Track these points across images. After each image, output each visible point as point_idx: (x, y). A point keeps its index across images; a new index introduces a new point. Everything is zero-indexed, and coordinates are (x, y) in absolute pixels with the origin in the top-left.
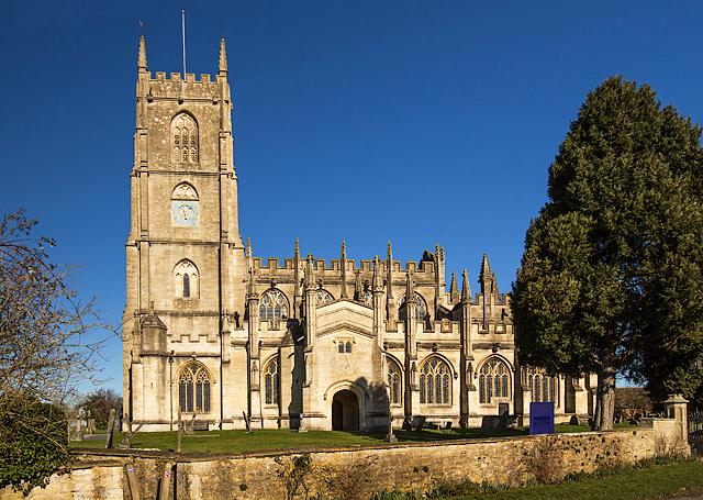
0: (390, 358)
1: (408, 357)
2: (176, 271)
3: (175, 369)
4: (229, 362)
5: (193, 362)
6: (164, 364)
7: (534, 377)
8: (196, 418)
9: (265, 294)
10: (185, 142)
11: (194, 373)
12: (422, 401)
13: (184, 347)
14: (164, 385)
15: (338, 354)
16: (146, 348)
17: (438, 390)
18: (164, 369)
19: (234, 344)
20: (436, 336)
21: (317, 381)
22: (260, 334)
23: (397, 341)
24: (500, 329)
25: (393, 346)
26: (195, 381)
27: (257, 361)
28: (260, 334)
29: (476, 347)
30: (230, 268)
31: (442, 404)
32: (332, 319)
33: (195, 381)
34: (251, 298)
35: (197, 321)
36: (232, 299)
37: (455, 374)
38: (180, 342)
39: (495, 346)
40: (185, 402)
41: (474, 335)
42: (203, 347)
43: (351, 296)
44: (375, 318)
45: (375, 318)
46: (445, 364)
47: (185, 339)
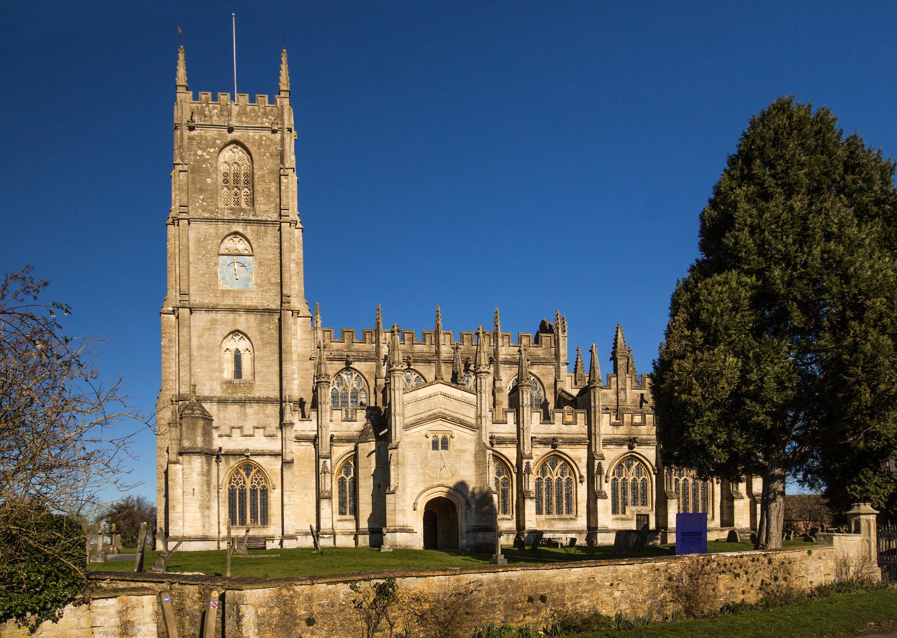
1: (520, 456)
2: (224, 347)
5: (246, 462)
7: (681, 482)
10: (237, 182)
11: (248, 475)
12: (539, 511)
14: (209, 491)
15: (431, 452)
16: (186, 444)
17: (559, 498)
19: (299, 439)
20: (556, 428)
22: (332, 427)
25: (502, 441)
26: (248, 486)
27: (328, 461)
29: (608, 442)
33: (248, 486)
34: (319, 382)
38: (229, 436)
39: (632, 442)
41: (605, 427)
42: (259, 442)
43: (448, 377)
44: (478, 406)
46: (568, 464)
47: (236, 433)
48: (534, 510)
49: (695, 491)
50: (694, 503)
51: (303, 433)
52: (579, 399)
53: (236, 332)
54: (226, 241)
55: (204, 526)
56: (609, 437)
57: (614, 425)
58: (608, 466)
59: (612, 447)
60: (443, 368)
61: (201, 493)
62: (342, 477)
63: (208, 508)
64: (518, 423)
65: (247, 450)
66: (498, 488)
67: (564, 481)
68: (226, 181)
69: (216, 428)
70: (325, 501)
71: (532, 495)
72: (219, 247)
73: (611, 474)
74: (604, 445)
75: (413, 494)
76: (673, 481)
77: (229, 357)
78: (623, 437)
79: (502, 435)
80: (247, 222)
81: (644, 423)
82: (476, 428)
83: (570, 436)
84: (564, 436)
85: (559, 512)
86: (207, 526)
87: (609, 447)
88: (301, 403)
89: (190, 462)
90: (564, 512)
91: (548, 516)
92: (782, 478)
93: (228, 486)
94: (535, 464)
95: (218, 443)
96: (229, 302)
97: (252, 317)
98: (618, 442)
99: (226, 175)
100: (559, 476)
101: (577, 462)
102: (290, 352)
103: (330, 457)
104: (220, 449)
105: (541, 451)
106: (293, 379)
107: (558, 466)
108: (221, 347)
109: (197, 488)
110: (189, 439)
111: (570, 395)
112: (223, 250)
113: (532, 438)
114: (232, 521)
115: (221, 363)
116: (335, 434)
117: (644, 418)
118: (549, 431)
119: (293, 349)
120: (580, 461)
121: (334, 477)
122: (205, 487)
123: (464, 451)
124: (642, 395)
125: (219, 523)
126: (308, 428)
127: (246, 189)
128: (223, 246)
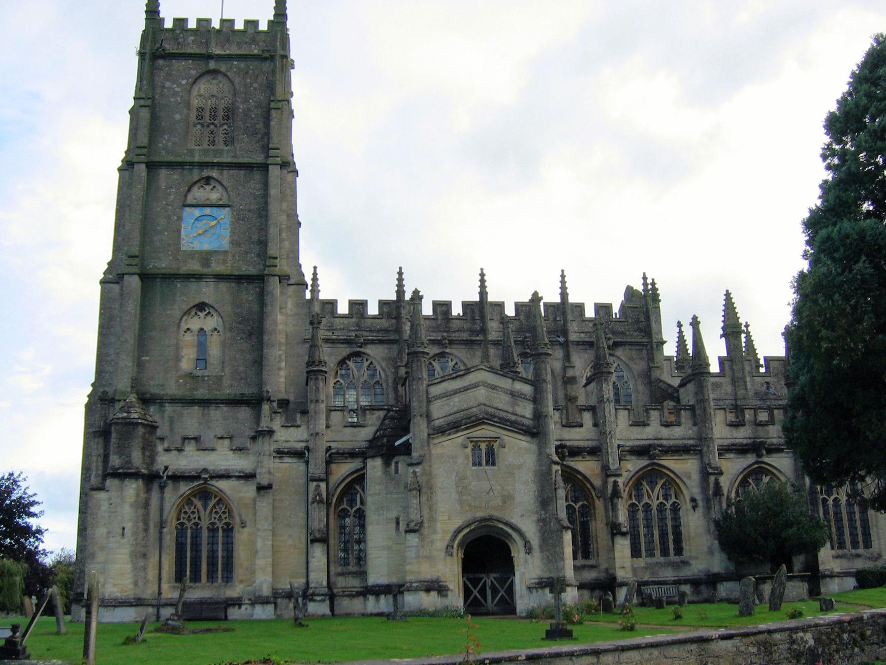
0: (570, 476)
1: (607, 472)
2: (184, 326)
3: (172, 496)
4: (269, 487)
5: (202, 486)
6: (148, 490)
7: (830, 502)
8: (566, 523)
9: (342, 363)
10: (214, 117)
11: (205, 506)
12: (636, 552)
13: (190, 460)
14: (146, 530)
15: (472, 470)
16: (115, 461)
17: (663, 535)
18: (146, 505)
19: (281, 453)
20: (653, 431)
21: (433, 520)
22: (329, 435)
23: (581, 444)
24: (763, 416)
25: (575, 452)
26: (205, 524)
27: (323, 485)
28: (329, 435)
29: (725, 450)
30: (280, 318)
31: (861, 551)
32: (457, 402)
33: (205, 524)
34: (313, 371)
35: (217, 414)
36: (282, 373)
37: (693, 500)
38: (180, 450)
39: (755, 448)
40: (186, 569)
41: (720, 430)
42: (222, 458)
43: (496, 363)
44: (537, 400)
45: (537, 400)
46: (672, 484)
47: (190, 448)
48: (628, 552)
49: (851, 520)
50: (851, 534)
51: (287, 445)
53: (201, 306)
54: (195, 189)
55: (136, 584)
56: (726, 442)
57: (732, 425)
58: (728, 483)
59: (732, 456)
60: (492, 351)
61: (135, 533)
62: (344, 509)
63: (144, 556)
64: (596, 425)
65: (205, 470)
66: (571, 520)
67: (668, 506)
68: (200, 117)
69: (162, 439)
71: (624, 530)
72: (186, 196)
73: (733, 495)
74: (720, 455)
75: (445, 532)
76: (820, 502)
77: (189, 339)
78: (745, 441)
79: (576, 443)
80: (221, 166)
81: (771, 421)
82: (535, 431)
83: (672, 443)
84: (665, 442)
85: (665, 552)
86: (140, 583)
87: (728, 456)
88: (284, 403)
89: (121, 489)
90: (484, 462)
91: (649, 560)
92: (862, 479)
93: (175, 523)
94: (626, 485)
95: (169, 461)
96: (195, 266)
97: (223, 286)
98: (741, 450)
99: (200, 110)
100: (661, 500)
101: (685, 479)
103: (326, 480)
104: (166, 468)
105: (633, 465)
106: (280, 369)
107: (659, 486)
108: (179, 326)
109: (129, 526)
110: (120, 454)
111: (670, 386)
112: (190, 199)
113: (619, 446)
114: (179, 577)
115: (178, 348)
116: (333, 445)
117: (771, 415)
118: (644, 436)
119: (280, 327)
120: (689, 478)
121: (332, 509)
123: (520, 467)
125: (160, 579)
126: (291, 436)
128: (190, 197)
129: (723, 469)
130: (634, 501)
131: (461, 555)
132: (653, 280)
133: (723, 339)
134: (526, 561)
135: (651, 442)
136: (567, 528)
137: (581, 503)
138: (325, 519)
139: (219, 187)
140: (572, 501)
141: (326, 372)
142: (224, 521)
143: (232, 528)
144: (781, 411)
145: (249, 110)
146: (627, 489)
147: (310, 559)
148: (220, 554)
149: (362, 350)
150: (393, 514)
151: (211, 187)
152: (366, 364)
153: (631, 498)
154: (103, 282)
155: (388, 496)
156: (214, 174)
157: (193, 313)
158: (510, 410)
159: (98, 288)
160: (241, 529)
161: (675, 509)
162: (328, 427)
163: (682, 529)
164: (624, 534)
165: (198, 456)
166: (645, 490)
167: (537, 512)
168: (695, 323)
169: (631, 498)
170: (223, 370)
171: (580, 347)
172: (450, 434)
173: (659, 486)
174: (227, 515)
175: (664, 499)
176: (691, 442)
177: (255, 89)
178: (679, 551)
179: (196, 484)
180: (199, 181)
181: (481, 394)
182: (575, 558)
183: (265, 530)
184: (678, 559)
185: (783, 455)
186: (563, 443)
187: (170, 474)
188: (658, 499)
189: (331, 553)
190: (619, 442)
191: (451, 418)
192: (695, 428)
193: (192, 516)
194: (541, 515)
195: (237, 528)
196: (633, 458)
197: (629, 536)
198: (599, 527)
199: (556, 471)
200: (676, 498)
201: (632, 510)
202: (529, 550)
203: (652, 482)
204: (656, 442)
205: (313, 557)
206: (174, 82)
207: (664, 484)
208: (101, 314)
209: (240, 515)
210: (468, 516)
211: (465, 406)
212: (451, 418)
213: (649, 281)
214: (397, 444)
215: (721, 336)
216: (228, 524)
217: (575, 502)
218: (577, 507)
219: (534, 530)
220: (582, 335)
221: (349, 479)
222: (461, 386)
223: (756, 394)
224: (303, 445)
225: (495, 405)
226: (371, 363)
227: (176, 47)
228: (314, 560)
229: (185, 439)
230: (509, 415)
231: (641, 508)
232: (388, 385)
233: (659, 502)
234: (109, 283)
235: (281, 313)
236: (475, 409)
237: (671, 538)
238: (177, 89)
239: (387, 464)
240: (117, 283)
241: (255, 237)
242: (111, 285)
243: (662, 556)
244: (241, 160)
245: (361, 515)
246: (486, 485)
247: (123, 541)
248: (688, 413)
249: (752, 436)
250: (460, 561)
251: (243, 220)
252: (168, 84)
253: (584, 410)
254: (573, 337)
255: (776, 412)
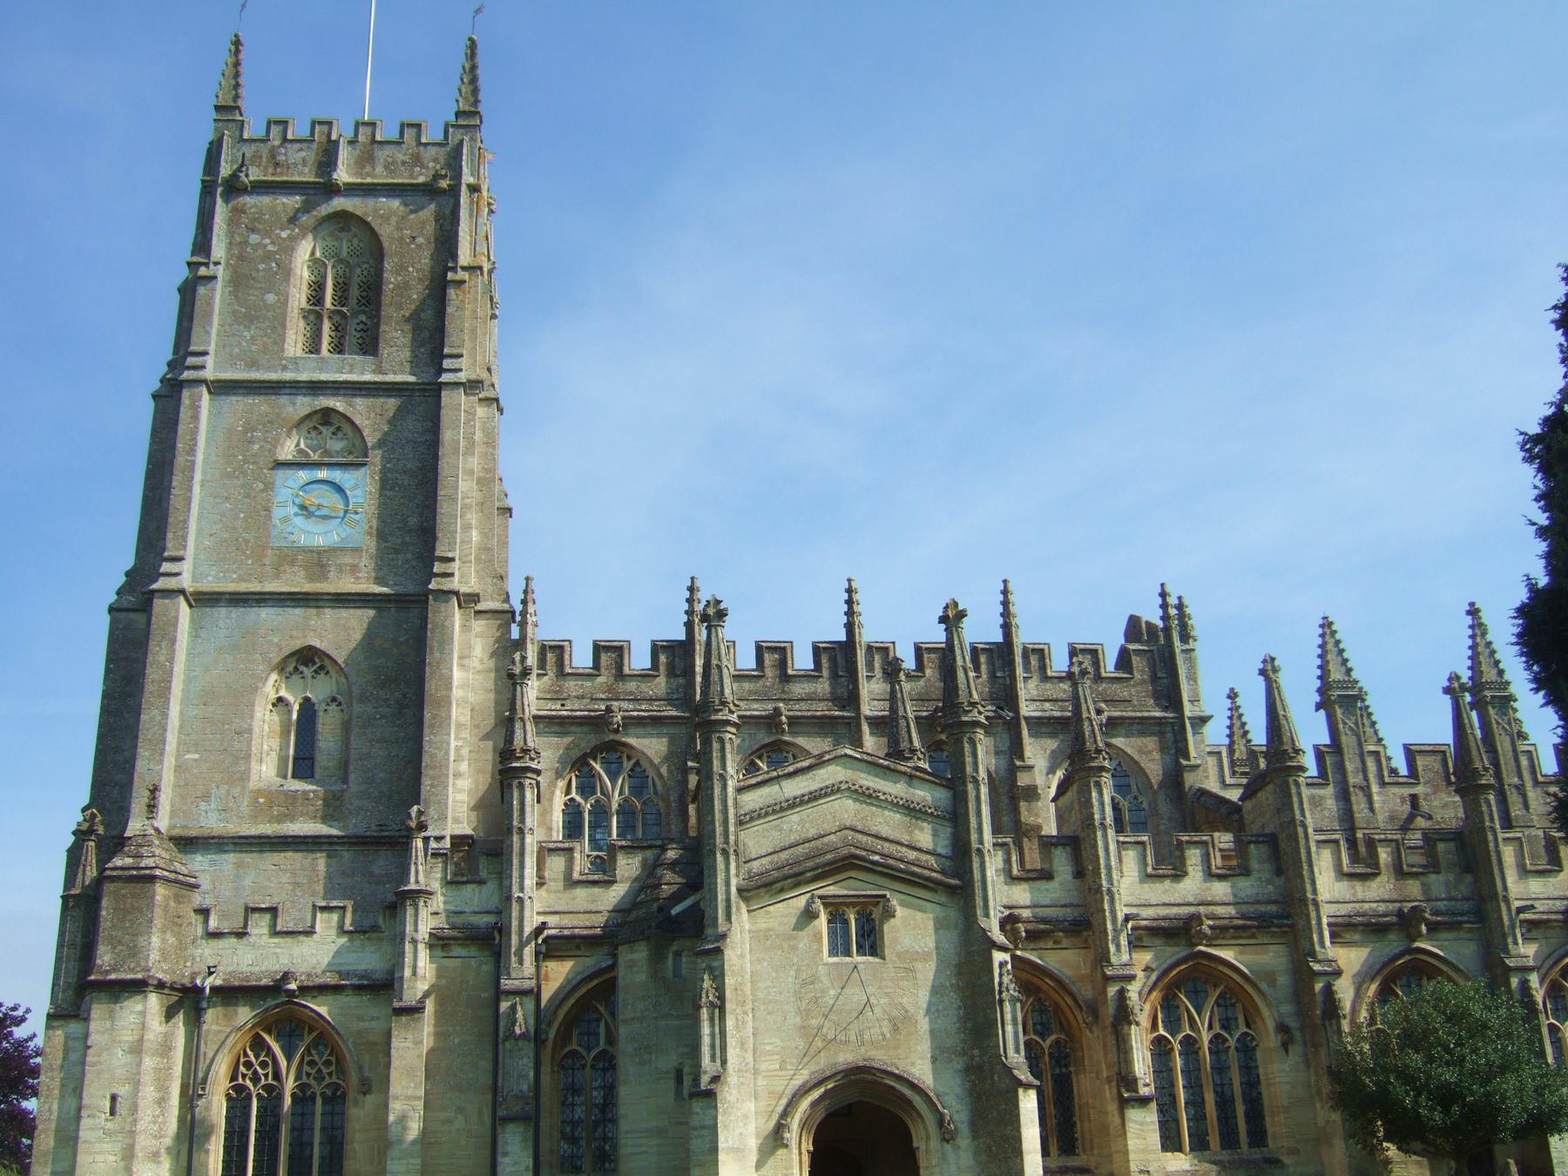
17: (1225, 1103)
30: (457, 675)
32: (797, 824)
38: (241, 934)
44: (955, 817)
45: (955, 817)
47: (259, 927)
48: (1155, 1138)
52: (1248, 805)
56: (1344, 909)
59: (1357, 937)
62: (574, 1053)
64: (1079, 873)
67: (1232, 1043)
70: (511, 1127)
71: (1144, 1091)
73: (1363, 1015)
74: (1333, 935)
76: (1545, 1031)
78: (1382, 908)
87: (1348, 937)
89: (112, 1017)
94: (1144, 996)
96: (296, 581)
100: (1217, 1029)
101: (1263, 986)
102: (446, 702)
106: (457, 775)
107: (1211, 1001)
116: (552, 920)
120: (1272, 981)
122: (1377, 967)
124: (1414, 799)
127: (363, 318)
129: (1341, 963)
130: (1162, 1032)
131: (808, 1146)
132: (1180, 598)
133: (1322, 712)
134: (944, 1157)
135: (1192, 909)
136: (1028, 1086)
137: (1053, 1037)
138: (532, 1074)
139: (346, 427)
140: (1036, 1032)
141: (538, 772)
142: (328, 1080)
143: (344, 1095)
144: (1452, 845)
145: (406, 286)
146: (1147, 1007)
147: (500, 1159)
148: (317, 1141)
149: (617, 737)
150: (668, 1061)
151: (332, 429)
152: (627, 765)
153: (1154, 1026)
154: (112, 609)
155: (662, 1023)
156: (338, 404)
157: (290, 669)
158: (905, 838)
159: (105, 621)
160: (361, 1097)
161: (1247, 1049)
162: (540, 884)
163: (1263, 1088)
164: (1144, 1101)
165: (277, 946)
166: (1182, 1008)
167: (964, 1053)
168: (1268, 671)
169: (1154, 1026)
170: (345, 780)
171: (1044, 729)
172: (782, 890)
173: (1211, 1001)
174: (333, 1068)
175: (1223, 1027)
176: (1272, 908)
177: (419, 247)
178: (1258, 1135)
179: (271, 1002)
180: (308, 416)
181: (845, 809)
182: (1045, 1152)
183: (409, 1098)
184: (1257, 1154)
185: (1462, 934)
186: (1016, 912)
187: (219, 982)
188: (1210, 1027)
189: (545, 1145)
190: (1127, 910)
191: (784, 855)
192: (1279, 881)
193: (325, 1071)
194: (972, 1057)
195: (352, 1094)
196: (1158, 942)
197: (1153, 1105)
198: (1091, 1086)
199: (1002, 965)
200: (1248, 1026)
201: (1160, 1049)
202: (947, 1136)
203: (1196, 992)
204: (1202, 909)
205: (506, 1154)
206: (267, 234)
207: (1220, 997)
208: (108, 671)
209: (361, 1068)
210: (824, 1062)
211: (812, 832)
212: (784, 855)
213: (1172, 600)
214: (674, 912)
215: (1318, 707)
216: (337, 1086)
217: (1043, 1036)
218: (1046, 1044)
219: (958, 1090)
220: (1047, 705)
221: (583, 990)
222: (806, 790)
223: (1392, 818)
224: (491, 919)
225: (874, 830)
226: (637, 763)
227: (270, 170)
228: (506, 1160)
229: (250, 910)
230: (904, 849)
231: (1177, 1047)
232: (668, 806)
233: (1212, 1033)
234: (127, 610)
235: (462, 666)
236: (832, 837)
237: (1240, 1109)
238: (270, 248)
239: (657, 958)
240: (144, 610)
241: (413, 521)
242: (132, 615)
243: (1223, 1147)
244: (390, 378)
245: (607, 1062)
246: (855, 995)
247: (109, 1125)
248: (1264, 849)
249: (1395, 896)
250: (806, 1159)
251: (392, 489)
252: (254, 238)
253: (1056, 845)
254: (1026, 709)
255: (1441, 846)
